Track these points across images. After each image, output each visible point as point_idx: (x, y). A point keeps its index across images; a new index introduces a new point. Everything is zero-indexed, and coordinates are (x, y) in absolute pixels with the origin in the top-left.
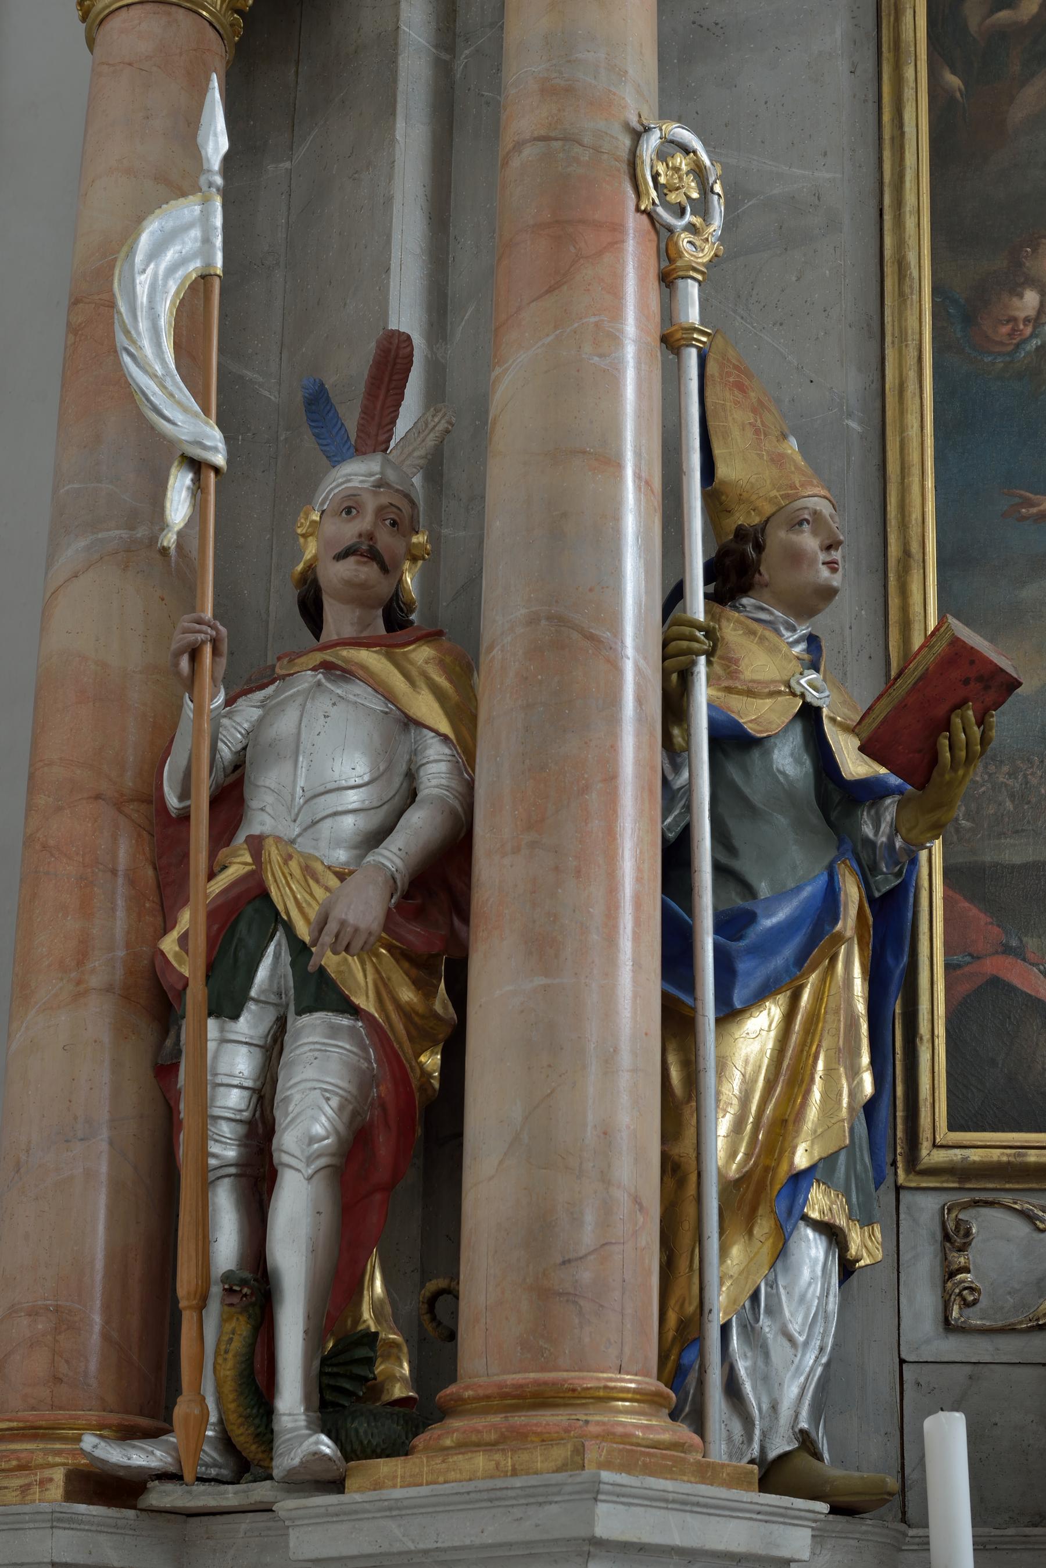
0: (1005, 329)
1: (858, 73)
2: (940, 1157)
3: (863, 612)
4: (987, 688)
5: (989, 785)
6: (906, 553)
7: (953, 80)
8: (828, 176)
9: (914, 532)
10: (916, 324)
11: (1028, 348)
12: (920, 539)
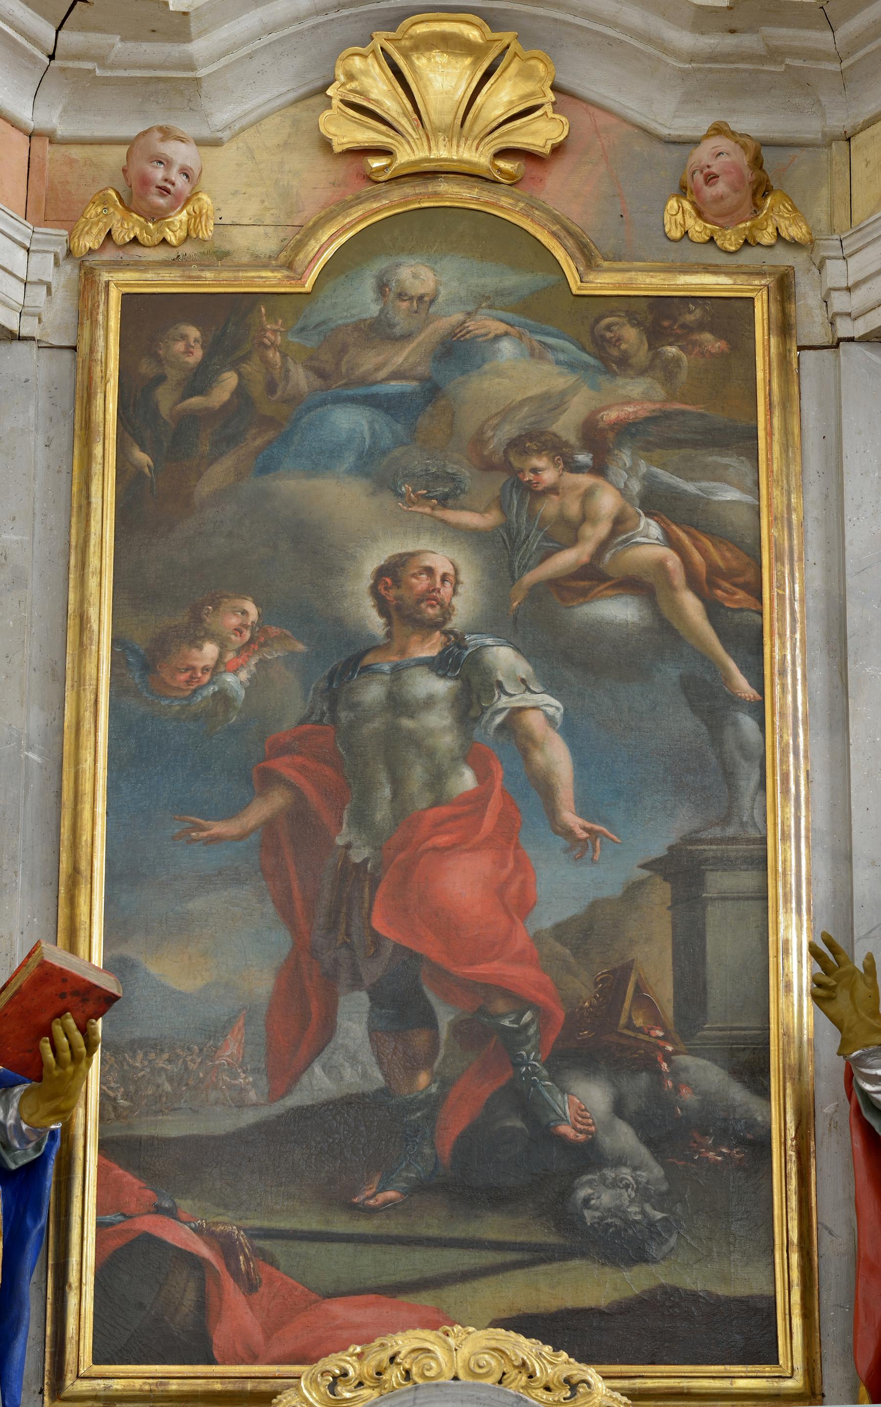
0: (183, 677)
1: (53, 446)
2: (83, 1386)
3: (35, 920)
4: (84, 1001)
5: (148, 1070)
6: (75, 870)
7: (142, 458)
8: (15, 538)
9: (84, 851)
10: (94, 672)
11: (205, 693)
12: (89, 858)
